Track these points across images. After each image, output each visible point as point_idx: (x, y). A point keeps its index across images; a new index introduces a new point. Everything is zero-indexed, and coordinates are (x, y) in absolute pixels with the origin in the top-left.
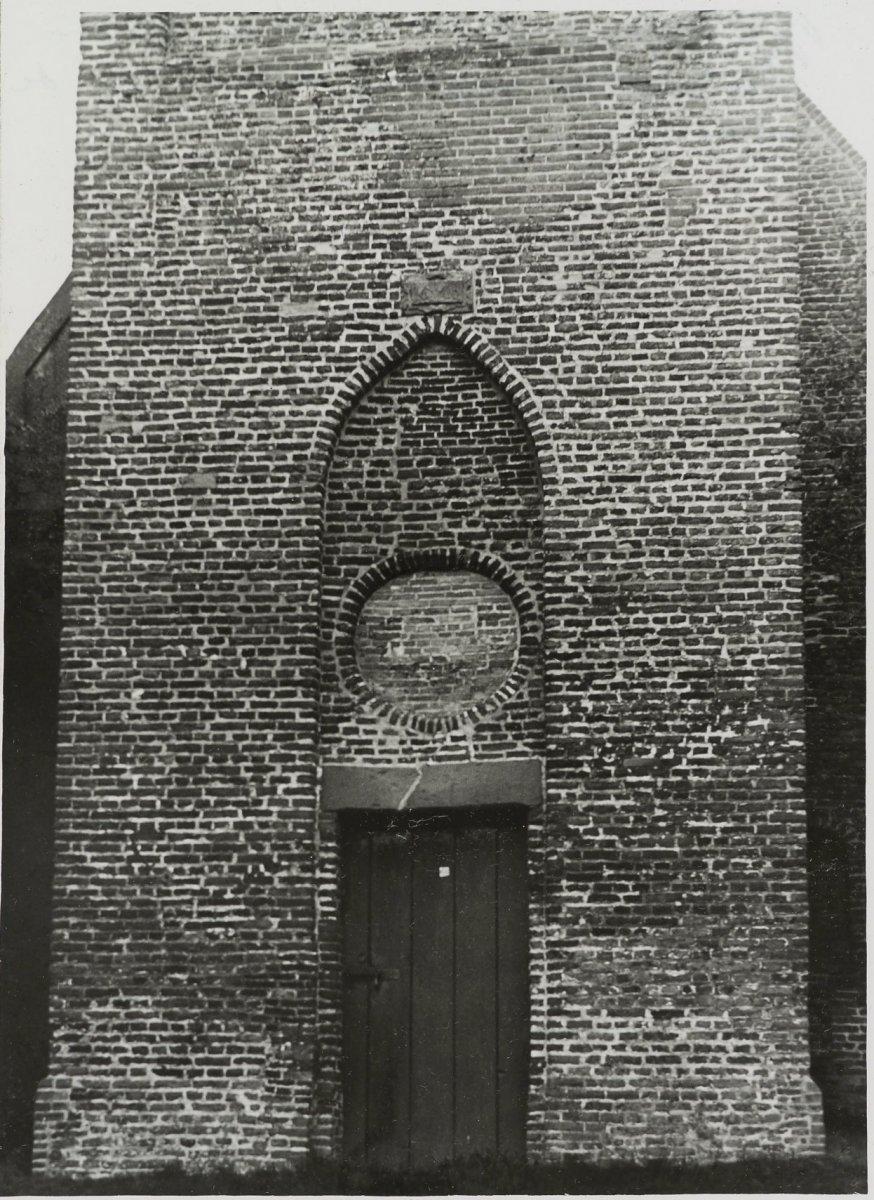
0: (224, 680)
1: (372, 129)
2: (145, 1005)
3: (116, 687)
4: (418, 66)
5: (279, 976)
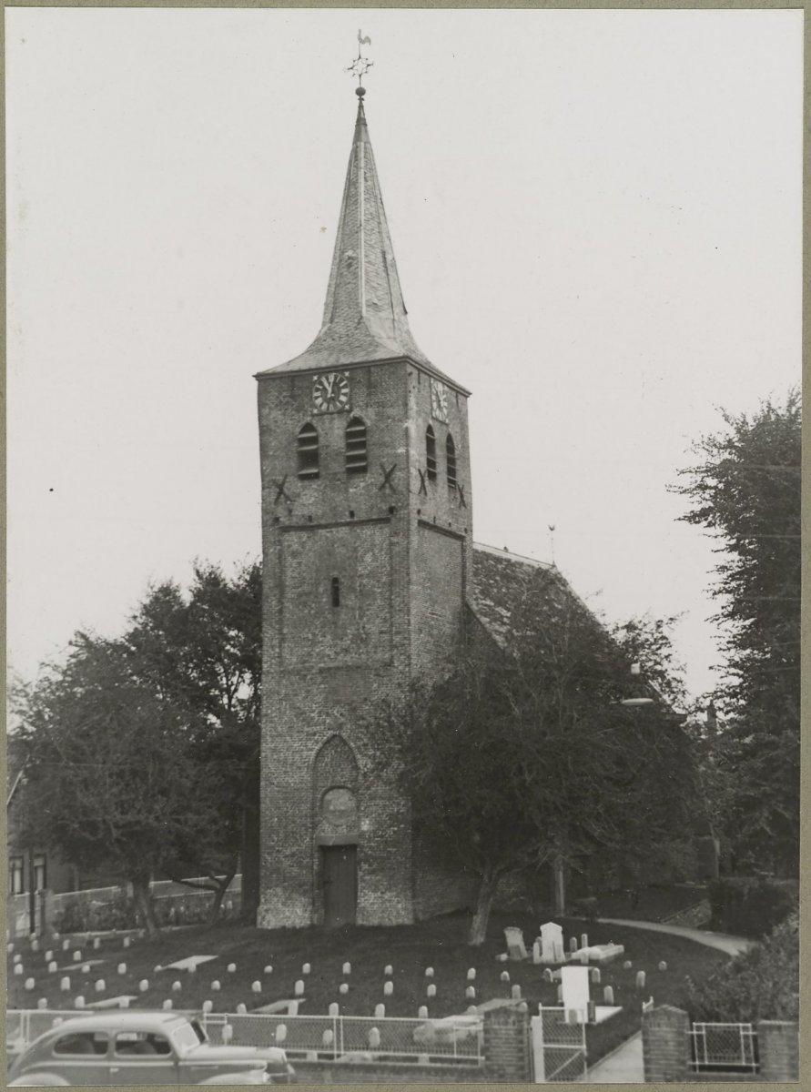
0: (293, 816)
1: (323, 686)
2: (279, 890)
3: (272, 817)
4: (332, 671)
5: (304, 884)
